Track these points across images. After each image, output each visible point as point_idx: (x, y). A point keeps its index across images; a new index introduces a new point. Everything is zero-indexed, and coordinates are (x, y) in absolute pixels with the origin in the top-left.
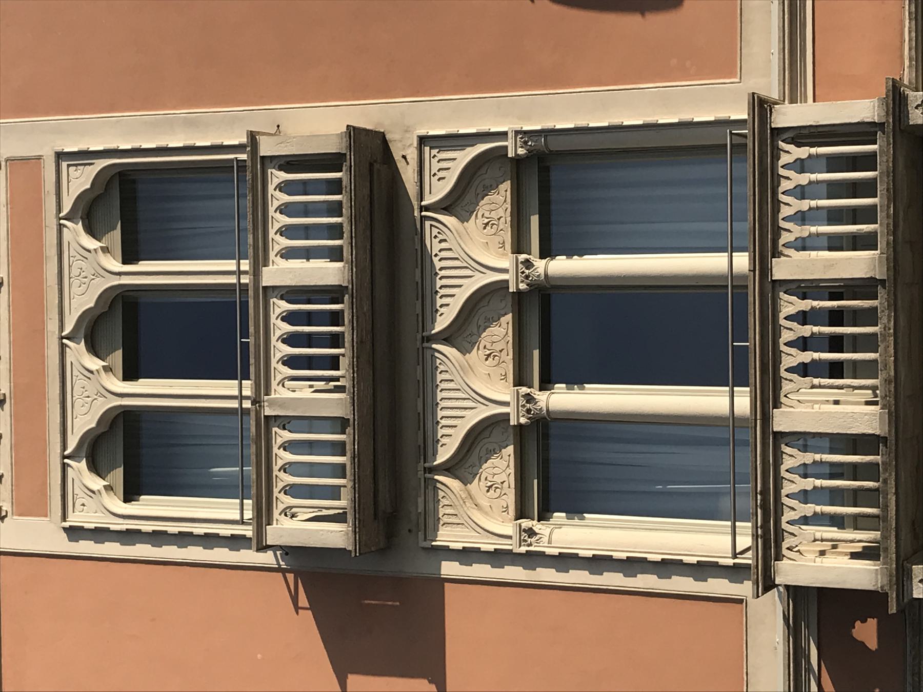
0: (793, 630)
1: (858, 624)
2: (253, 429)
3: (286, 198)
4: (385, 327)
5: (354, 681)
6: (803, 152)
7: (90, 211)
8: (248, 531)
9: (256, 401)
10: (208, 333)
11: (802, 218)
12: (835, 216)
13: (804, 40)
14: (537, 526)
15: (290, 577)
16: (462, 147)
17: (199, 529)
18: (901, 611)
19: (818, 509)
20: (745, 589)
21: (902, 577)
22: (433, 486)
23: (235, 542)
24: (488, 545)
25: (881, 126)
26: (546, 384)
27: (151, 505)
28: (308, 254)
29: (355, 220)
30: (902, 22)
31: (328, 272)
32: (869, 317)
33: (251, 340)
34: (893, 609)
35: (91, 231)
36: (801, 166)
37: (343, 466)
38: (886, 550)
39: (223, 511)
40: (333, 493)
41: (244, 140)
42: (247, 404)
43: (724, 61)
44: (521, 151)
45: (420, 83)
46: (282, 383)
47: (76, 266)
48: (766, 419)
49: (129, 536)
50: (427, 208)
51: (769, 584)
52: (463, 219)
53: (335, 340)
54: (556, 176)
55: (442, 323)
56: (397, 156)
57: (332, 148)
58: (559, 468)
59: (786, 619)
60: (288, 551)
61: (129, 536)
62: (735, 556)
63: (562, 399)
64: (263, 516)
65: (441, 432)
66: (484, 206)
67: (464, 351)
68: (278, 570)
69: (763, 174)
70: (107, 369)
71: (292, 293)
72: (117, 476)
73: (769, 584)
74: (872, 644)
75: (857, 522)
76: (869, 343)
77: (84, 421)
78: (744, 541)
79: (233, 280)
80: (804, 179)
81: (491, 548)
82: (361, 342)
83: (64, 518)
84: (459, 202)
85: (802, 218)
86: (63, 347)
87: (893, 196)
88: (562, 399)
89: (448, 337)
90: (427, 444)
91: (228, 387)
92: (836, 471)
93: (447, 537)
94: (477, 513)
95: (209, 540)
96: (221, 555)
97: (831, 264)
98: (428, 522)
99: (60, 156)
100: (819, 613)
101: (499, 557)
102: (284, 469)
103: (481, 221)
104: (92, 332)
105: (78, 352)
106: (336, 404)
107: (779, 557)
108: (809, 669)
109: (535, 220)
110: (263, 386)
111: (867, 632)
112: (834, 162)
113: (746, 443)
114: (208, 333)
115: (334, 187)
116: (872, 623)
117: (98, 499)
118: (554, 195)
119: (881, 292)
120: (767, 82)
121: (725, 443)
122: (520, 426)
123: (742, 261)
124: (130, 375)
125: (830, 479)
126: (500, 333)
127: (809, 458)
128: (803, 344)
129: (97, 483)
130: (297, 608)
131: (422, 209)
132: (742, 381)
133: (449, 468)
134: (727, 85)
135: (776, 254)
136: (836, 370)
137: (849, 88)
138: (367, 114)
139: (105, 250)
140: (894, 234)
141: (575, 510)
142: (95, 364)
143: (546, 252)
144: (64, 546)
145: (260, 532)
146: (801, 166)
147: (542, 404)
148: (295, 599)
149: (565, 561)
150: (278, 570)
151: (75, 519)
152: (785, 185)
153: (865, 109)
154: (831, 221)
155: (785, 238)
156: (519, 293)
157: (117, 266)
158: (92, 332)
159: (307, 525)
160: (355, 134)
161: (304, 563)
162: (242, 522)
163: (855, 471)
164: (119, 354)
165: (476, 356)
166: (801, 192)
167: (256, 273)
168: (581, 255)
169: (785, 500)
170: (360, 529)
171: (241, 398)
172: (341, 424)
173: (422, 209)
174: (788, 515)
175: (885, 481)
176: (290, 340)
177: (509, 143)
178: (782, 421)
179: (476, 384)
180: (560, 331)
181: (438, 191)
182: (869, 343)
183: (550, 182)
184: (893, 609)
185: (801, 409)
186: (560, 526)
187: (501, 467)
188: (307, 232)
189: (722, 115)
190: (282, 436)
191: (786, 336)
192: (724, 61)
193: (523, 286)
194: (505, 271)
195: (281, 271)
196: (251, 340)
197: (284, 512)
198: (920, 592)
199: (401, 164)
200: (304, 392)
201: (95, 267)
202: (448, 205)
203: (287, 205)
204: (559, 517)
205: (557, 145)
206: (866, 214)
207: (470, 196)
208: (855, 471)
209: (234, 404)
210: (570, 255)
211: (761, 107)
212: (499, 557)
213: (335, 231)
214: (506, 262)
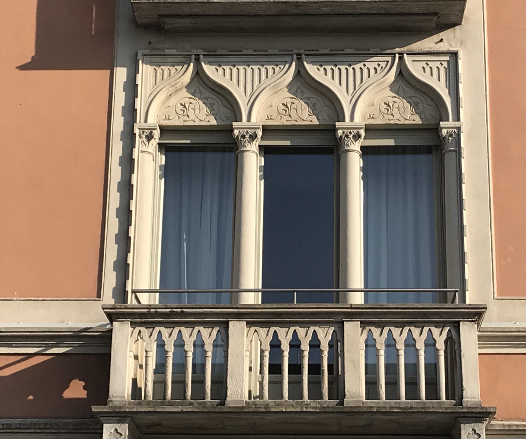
0: (77, 335)
6: (441, 345)
11: (391, 344)
14: (155, 142)
16: (448, 86)
18: (93, 415)
20: (108, 298)
21: (119, 416)
26: (264, 150)
34: (95, 409)
36: (431, 344)
38: (140, 404)
44: (444, 132)
48: (239, 316)
50: (401, 58)
51: (112, 317)
52: (392, 87)
55: (312, 69)
56: (442, 35)
58: (199, 158)
59: (86, 330)
62: (134, 292)
63: (253, 163)
73: (112, 317)
74: (67, 394)
75: (160, 383)
78: (145, 299)
81: (137, 106)
84: (407, 84)
85: (391, 344)
87: (406, 412)
88: (253, 163)
89: (301, 74)
90: (217, 57)
92: (199, 369)
93: (146, 72)
94: (165, 95)
97: (356, 365)
98: (157, 58)
100: (92, 355)
101: (130, 112)
103: (390, 100)
107: (134, 325)
109: (390, 142)
111: (76, 390)
113: (219, 301)
116: (83, 394)
118: (409, 158)
121: (219, 284)
122: (232, 130)
123: (357, 299)
126: (304, 115)
127: (209, 348)
128: (295, 345)
135: (364, 324)
136: (275, 369)
137: (487, 384)
141: (168, 172)
143: (365, 151)
146: (431, 344)
147: (249, 147)
149: (128, 164)
152: (416, 332)
153: (473, 391)
155: (376, 332)
156: (334, 130)
165: (286, 96)
169: (176, 330)
174: (165, 332)
175: (191, 404)
177: (451, 123)
178: (237, 328)
181: (415, 67)
184: (95, 409)
186: (155, 160)
187: (200, 115)
191: (301, 332)
193: (340, 133)
199: (436, 38)
202: (403, 74)
207: (410, 92)
208: (199, 382)
210: (364, 169)
212: (130, 112)
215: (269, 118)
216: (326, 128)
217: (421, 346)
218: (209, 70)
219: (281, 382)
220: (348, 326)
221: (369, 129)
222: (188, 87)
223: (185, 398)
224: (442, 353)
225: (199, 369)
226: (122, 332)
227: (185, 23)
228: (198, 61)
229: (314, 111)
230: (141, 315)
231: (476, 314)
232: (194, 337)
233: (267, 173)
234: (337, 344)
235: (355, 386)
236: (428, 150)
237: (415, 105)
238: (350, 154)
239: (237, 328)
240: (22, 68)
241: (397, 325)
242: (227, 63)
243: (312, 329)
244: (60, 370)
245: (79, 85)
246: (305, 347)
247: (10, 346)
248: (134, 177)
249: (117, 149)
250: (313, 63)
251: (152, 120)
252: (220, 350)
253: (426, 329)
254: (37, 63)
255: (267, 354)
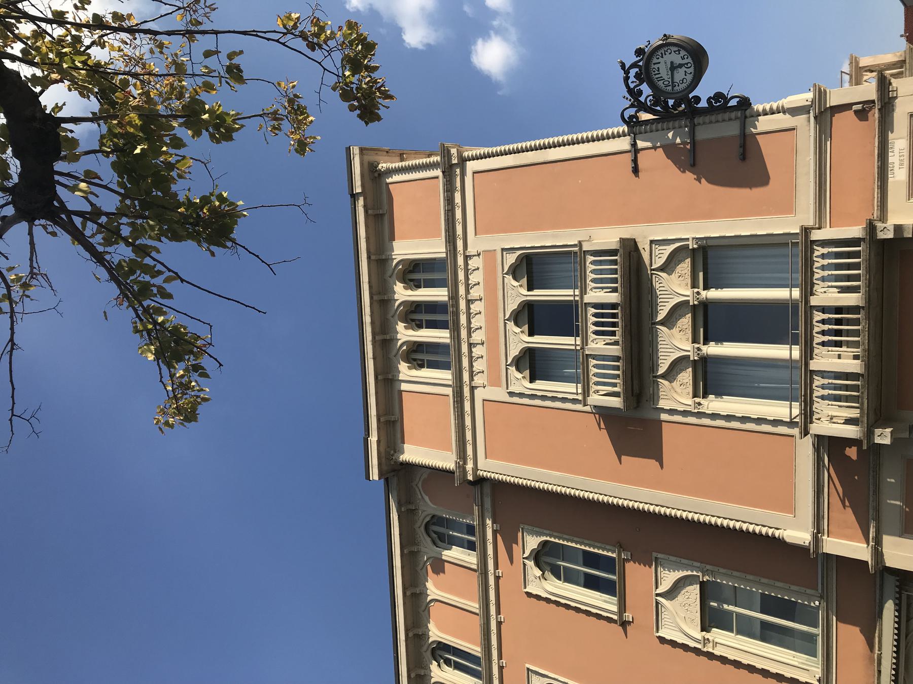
0: (817, 449)
1: (847, 449)
3: (594, 267)
4: (636, 316)
5: (624, 458)
7: (514, 271)
8: (580, 397)
10: (562, 318)
13: (825, 174)
15: (597, 416)
16: (669, 244)
17: (560, 396)
18: (869, 447)
20: (796, 431)
21: (870, 434)
23: (574, 401)
25: (863, 239)
26: (706, 342)
27: (541, 385)
29: (622, 276)
30: (874, 189)
32: (856, 322)
34: (865, 447)
35: (515, 278)
36: (823, 256)
39: (569, 389)
42: (578, 348)
44: (695, 246)
45: (650, 219)
47: (510, 292)
50: (654, 270)
53: (614, 325)
54: (710, 253)
55: (660, 317)
56: (641, 248)
58: (711, 377)
59: (814, 445)
63: (713, 349)
67: (670, 328)
68: (592, 413)
69: (806, 260)
70: (522, 332)
71: (596, 306)
72: (527, 373)
73: (806, 432)
77: (514, 352)
78: (796, 411)
81: (682, 409)
82: (626, 326)
84: (668, 266)
87: (869, 270)
88: (713, 349)
90: (654, 366)
93: (663, 404)
94: (676, 395)
95: (564, 400)
98: (655, 398)
99: (503, 250)
100: (830, 447)
102: (592, 272)
103: (677, 275)
104: (516, 317)
105: (511, 325)
106: (616, 350)
108: (824, 465)
109: (701, 274)
110: (585, 342)
111: (852, 452)
113: (796, 368)
114: (562, 318)
115: (615, 262)
117: (520, 382)
118: (709, 261)
120: (810, 222)
123: (796, 293)
124: (531, 334)
125: (836, 346)
126: (686, 321)
128: (823, 333)
129: (519, 376)
130: (600, 428)
133: (663, 376)
134: (790, 218)
136: (838, 344)
139: (521, 286)
140: (869, 287)
141: (719, 394)
142: (518, 330)
143: (706, 288)
144: (508, 399)
146: (823, 256)
148: (599, 425)
149: (714, 416)
150: (592, 413)
151: (511, 389)
152: (816, 265)
153: (856, 231)
154: (835, 389)
157: (525, 292)
158: (516, 317)
160: (622, 241)
161: (603, 413)
162: (577, 394)
164: (525, 279)
165: (675, 331)
166: (823, 268)
167: (582, 298)
168: (722, 288)
169: (815, 399)
170: (625, 401)
172: (617, 359)
173: (651, 270)
175: (862, 393)
176: (596, 324)
177: (690, 243)
178: (814, 365)
179: (675, 343)
180: (711, 321)
181: (659, 262)
183: (708, 259)
184: (865, 447)
185: (823, 360)
186: (712, 401)
191: (816, 329)
192: (787, 207)
193: (696, 303)
197: (594, 392)
201: (518, 293)
202: (662, 269)
204: (711, 397)
205: (710, 243)
207: (672, 264)
208: (847, 388)
209: (573, 348)
210: (717, 288)
212: (685, 413)
214: (689, 292)
215: (688, 340)
220: (812, 303)
226: (817, 428)
227: (636, 382)
228: (656, 377)
229: (683, 315)
233: (720, 340)
235: (852, 299)
237: (680, 262)
238: (708, 297)
240: (662, 467)
242: (657, 362)
246: (826, 327)
247: (823, 486)
248: (722, 413)
250: (657, 316)
252: (825, 374)
254: (660, 460)
255: (830, 284)
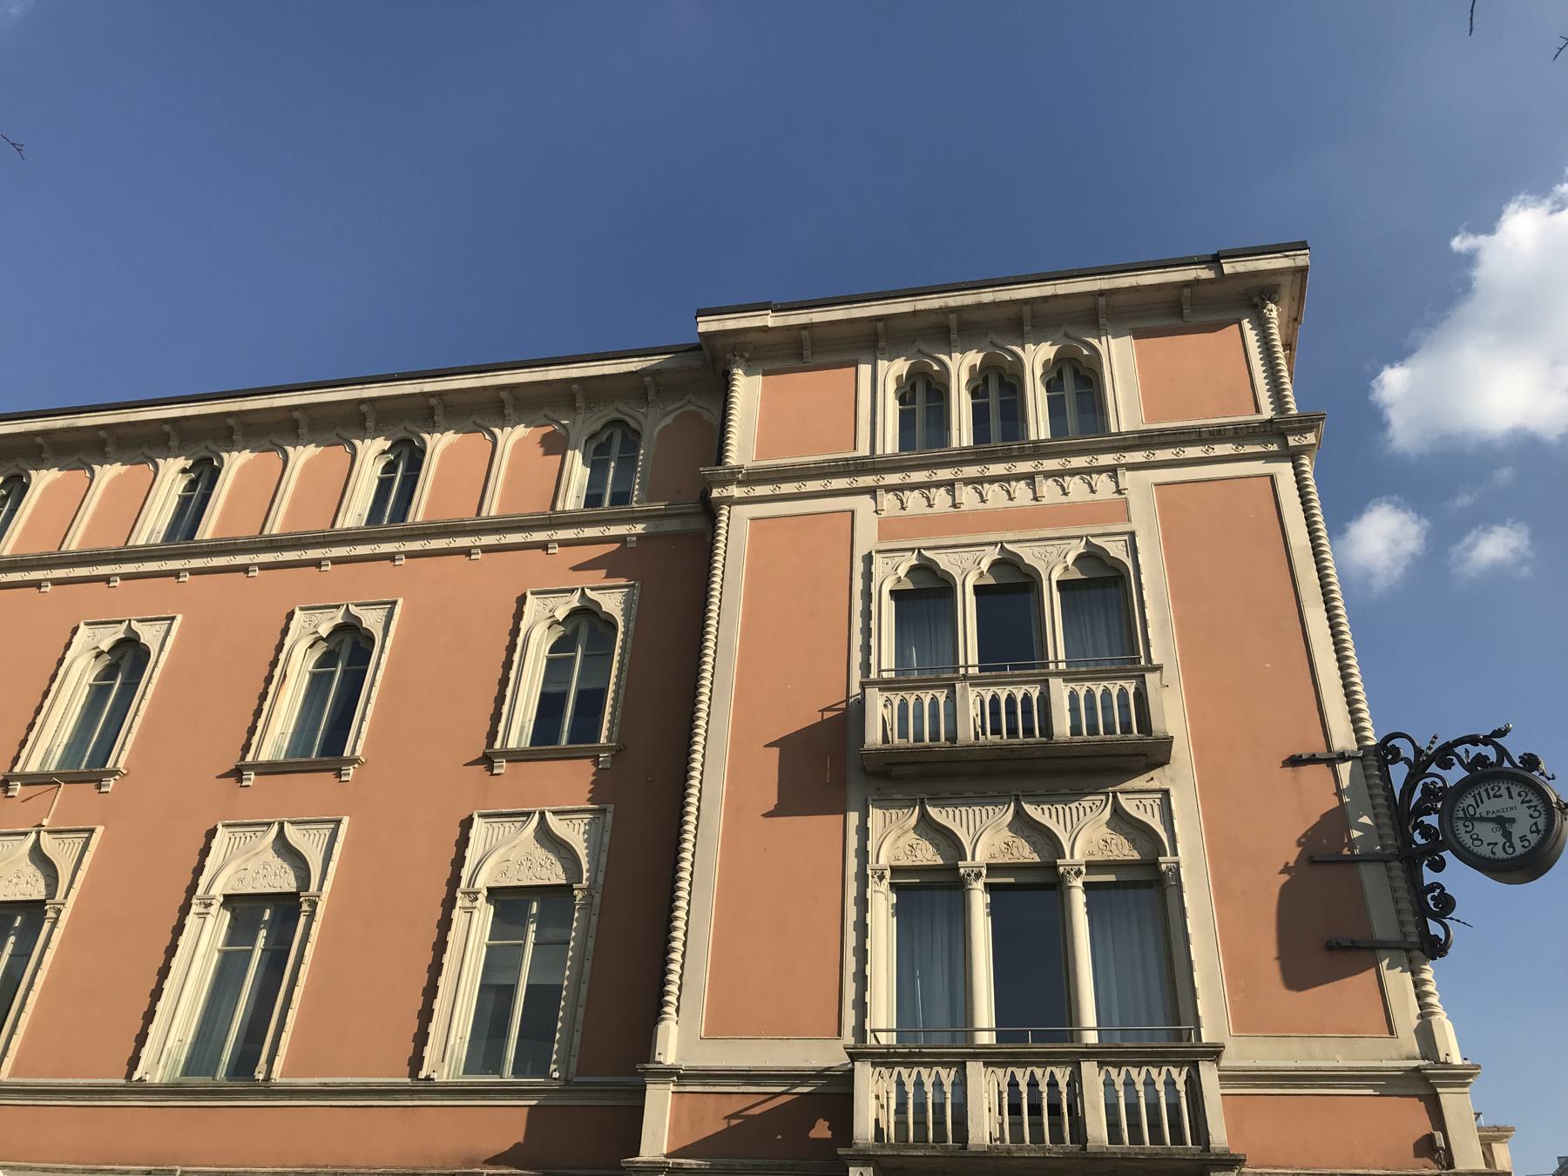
0: (821, 1074)
2: (945, 675)
4: (1026, 768)
6: (1181, 1086)
7: (1093, 557)
8: (873, 675)
9: (965, 677)
11: (1129, 1083)
12: (1133, 1109)
13: (1300, 1087)
14: (886, 882)
15: (843, 705)
16: (1163, 823)
17: (873, 642)
19: (911, 1095)
20: (849, 1038)
21: (864, 1159)
22: (911, 805)
23: (866, 667)
24: (871, 846)
26: (989, 888)
27: (888, 608)
28: (1074, 709)
31: (1062, 726)
32: (1057, 1137)
33: (1009, 672)
34: (840, 1151)
35: (1079, 558)
36: (1170, 1083)
37: (922, 740)
38: (883, 1147)
40: (903, 734)
41: (1155, 662)
42: (962, 671)
43: (1245, 1024)
44: (1164, 867)
45: (1209, 789)
46: (979, 694)
48: (975, 1056)
49: (867, 595)
50: (1115, 797)
51: (854, 1057)
52: (1108, 824)
53: (1012, 732)
55: (1030, 809)
57: (1156, 725)
58: (929, 897)
59: (829, 1069)
60: (861, 703)
61: (867, 595)
62: (873, 1031)
63: (979, 900)
64: (885, 686)
65: (950, 810)
66: (1120, 840)
67: (1010, 826)
68: (848, 697)
71: (1045, 700)
73: (854, 1057)
74: (813, 1134)
75: (901, 1124)
76: (1037, 1136)
77: (944, 561)
78: (884, 1039)
79: (1051, 658)
80: (1160, 1087)
82: (1012, 750)
83: (878, 552)
84: (1122, 821)
85: (1129, 1083)
86: (995, 544)
87: (1151, 1158)
88: (979, 900)
89: (1020, 814)
90: (940, 801)
91: (973, 658)
92: (939, 1108)
93: (876, 815)
94: (894, 838)
95: (866, 649)
96: (857, 657)
97: (1095, 1108)
98: (885, 802)
99: (1132, 534)
100: (834, 1094)
101: (863, 854)
102: (918, 698)
104: (1007, 563)
105: (993, 554)
106: (967, 732)
107: (874, 1065)
109: (1112, 878)
110: (976, 682)
111: (821, 1130)
112: (1174, 1109)
113: (954, 1040)
115: (1126, 728)
116: (828, 1134)
117: (891, 573)
118: (1131, 892)
119: (1077, 1147)
121: (953, 1024)
122: (958, 869)
123: (1091, 1038)
124: (978, 590)
126: (1025, 853)
127: (948, 1088)
128: (1033, 1084)
129: (902, 572)
130: (822, 711)
131: (1114, 793)
132: (1001, 1037)
133: (924, 816)
135: (1101, 1065)
136: (1015, 1109)
137: (1233, 1128)
138: (1182, 750)
139: (1066, 568)
141: (899, 911)
142: (985, 566)
143: (1088, 886)
144: (859, 553)
145: (873, 683)
146: (1170, 1083)
147: (975, 885)
148: (828, 709)
149: (863, 903)
150: (848, 697)
151: (877, 558)
152: (1154, 1072)
155: (1113, 1071)
156: (1056, 867)
157: (1055, 578)
159: (880, 711)
160: (1167, 742)
162: (880, 671)
163: (940, 1123)
164: (993, 582)
165: (1007, 835)
167: (1058, 674)
169: (915, 1070)
170: (879, 753)
171: (966, 667)
172: (952, 737)
173: (1114, 793)
174: (905, 1072)
177: (1169, 858)
178: (974, 1069)
179: (987, 836)
180: (1030, 896)
181: (1129, 805)
182: (1037, 1136)
183: (1141, 890)
184: (840, 1151)
187: (927, 855)
188: (1091, 708)
189: (1204, 1022)
190: (942, 696)
191: (1038, 1072)
192: (1245, 1024)
193: (1061, 869)
194: (1072, 856)
195: (1060, 692)
196: (1009, 672)
197: (888, 700)
198: (854, 1174)
199: (1147, 776)
200: (974, 711)
201: (1053, 563)
202: (1118, 811)
203: (1110, 694)
205: (1171, 894)
206: (1156, 1137)
207: (1126, 828)
208: (940, 1123)
209: (961, 662)
210: (1087, 904)
211: (1214, 1053)
212: (863, 854)
213: (1093, 729)
214: (1079, 857)
215: (992, 857)
216: (1007, 859)
217: (1160, 1087)
218: (933, 812)
219: (1021, 1124)
221: (1089, 865)
222: (915, 828)
223: (927, 1141)
224: (1183, 1094)
225: (939, 1108)
226: (863, 1071)
230: (881, 1055)
231: (1214, 1053)
232: (933, 1078)
233: (994, 910)
234: (1075, 1080)
235: (1097, 1129)
236: (1148, 884)
237: (1132, 841)
239: (974, 1069)
240: (766, 815)
241: (1135, 1065)
242: (949, 805)
243: (1049, 1069)
244: (806, 1109)
245: (819, 827)
247: (758, 1085)
249: (852, 889)
251: (883, 861)
253: (1164, 1069)
255: (1005, 1095)
